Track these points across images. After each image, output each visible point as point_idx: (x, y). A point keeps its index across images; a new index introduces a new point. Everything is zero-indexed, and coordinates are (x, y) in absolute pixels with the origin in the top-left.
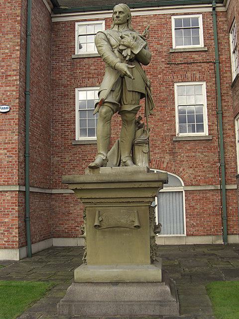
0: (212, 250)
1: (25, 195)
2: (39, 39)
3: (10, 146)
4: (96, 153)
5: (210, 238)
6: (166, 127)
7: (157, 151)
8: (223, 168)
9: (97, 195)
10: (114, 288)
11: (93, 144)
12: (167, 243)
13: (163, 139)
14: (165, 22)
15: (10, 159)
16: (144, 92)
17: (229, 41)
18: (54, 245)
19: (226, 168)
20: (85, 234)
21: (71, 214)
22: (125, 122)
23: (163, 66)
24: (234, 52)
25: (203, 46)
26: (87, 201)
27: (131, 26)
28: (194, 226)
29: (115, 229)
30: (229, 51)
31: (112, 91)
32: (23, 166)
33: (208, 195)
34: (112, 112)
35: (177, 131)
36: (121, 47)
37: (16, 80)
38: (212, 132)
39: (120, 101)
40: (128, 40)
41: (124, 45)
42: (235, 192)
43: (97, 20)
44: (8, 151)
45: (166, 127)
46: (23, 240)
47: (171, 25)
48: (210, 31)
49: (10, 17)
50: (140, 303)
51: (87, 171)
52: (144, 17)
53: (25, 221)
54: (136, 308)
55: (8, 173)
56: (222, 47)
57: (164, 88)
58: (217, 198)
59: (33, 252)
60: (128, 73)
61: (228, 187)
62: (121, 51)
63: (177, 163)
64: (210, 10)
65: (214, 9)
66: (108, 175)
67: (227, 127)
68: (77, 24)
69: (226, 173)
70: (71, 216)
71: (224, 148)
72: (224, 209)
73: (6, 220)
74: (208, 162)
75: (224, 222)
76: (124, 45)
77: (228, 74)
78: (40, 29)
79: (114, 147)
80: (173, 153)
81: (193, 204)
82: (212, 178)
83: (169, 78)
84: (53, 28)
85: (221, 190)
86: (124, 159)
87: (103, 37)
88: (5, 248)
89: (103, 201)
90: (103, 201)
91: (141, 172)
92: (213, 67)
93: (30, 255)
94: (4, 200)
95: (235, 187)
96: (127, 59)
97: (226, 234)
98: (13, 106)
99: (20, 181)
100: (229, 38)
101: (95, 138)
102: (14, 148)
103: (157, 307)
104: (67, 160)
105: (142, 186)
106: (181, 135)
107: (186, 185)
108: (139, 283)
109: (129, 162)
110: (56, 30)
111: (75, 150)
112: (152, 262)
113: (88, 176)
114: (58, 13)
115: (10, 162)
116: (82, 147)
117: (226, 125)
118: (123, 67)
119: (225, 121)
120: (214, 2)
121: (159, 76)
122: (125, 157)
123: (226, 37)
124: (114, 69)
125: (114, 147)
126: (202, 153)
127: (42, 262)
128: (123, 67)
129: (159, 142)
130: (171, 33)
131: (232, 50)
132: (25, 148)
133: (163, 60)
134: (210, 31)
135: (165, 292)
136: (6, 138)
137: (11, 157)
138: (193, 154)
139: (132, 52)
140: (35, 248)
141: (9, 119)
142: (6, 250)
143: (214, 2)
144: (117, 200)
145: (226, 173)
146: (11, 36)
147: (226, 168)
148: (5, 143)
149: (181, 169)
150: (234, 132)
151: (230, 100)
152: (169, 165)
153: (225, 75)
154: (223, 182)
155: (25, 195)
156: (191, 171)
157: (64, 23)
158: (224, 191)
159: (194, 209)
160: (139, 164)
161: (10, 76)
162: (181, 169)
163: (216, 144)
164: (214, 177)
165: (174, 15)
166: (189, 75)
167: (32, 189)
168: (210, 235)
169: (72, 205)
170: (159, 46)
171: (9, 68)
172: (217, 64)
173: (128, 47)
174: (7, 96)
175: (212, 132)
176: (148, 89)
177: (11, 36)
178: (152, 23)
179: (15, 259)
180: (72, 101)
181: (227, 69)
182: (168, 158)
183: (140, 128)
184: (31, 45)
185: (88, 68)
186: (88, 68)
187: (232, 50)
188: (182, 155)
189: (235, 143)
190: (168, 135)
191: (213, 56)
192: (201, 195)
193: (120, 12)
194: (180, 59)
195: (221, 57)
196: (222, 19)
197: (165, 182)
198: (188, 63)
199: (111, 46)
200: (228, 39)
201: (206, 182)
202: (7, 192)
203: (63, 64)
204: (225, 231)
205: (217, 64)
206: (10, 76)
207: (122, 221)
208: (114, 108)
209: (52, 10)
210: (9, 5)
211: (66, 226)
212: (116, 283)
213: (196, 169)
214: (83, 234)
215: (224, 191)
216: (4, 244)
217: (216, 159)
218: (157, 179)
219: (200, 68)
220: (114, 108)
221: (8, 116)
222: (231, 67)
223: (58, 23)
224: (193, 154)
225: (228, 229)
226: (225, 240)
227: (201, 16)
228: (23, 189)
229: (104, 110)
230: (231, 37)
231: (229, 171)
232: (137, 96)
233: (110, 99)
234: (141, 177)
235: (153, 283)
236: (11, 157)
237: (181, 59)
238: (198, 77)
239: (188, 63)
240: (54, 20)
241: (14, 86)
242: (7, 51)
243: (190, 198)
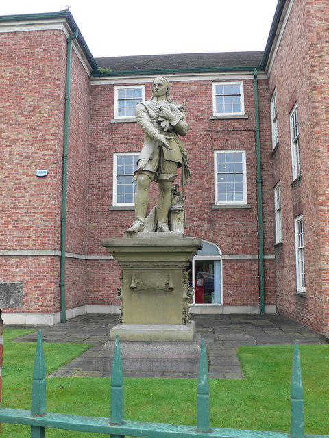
0: (246, 319)
1: (61, 259)
2: (78, 102)
3: (47, 210)
4: (134, 219)
5: (247, 307)
6: (205, 195)
7: (195, 219)
8: (261, 237)
9: (134, 259)
10: (147, 346)
11: (131, 211)
12: (203, 312)
13: (202, 207)
14: (206, 89)
15: (47, 224)
16: (181, 161)
17: (270, 109)
18: (88, 312)
19: (264, 238)
20: (121, 295)
21: (106, 281)
22: (163, 190)
23: (204, 133)
24: (275, 121)
25: (244, 114)
26: (123, 264)
27: (170, 97)
28: (231, 296)
29: (151, 291)
30: (270, 119)
31: (150, 160)
32: (59, 230)
33: (246, 264)
34: (150, 180)
35: (216, 200)
36: (160, 119)
37: (54, 144)
38: (251, 201)
39: (157, 170)
40: (167, 111)
41: (163, 117)
42: (273, 262)
43: (137, 84)
44: (44, 216)
45: (205, 195)
46: (57, 305)
47: (211, 92)
48: (251, 99)
49: (49, 81)
50: (171, 360)
51: (125, 236)
52: (184, 83)
53: (60, 286)
54: (168, 365)
55: (45, 237)
56: (263, 115)
57: (204, 155)
58: (255, 267)
59: (67, 318)
60: (167, 144)
61: (267, 257)
62: (159, 123)
63: (215, 232)
64: (252, 77)
65: (255, 76)
66: (144, 240)
67: (267, 196)
68: (116, 88)
69: (264, 243)
70: (106, 283)
71: (263, 217)
72: (262, 279)
73: (41, 285)
74: (246, 231)
75: (262, 292)
76: (163, 117)
77: (269, 143)
78: (79, 93)
79: (151, 213)
80: (211, 221)
81: (230, 273)
82: (250, 247)
83: (209, 145)
84: (92, 90)
85: (259, 259)
86: (160, 225)
87: (143, 108)
88: (39, 313)
89: (139, 264)
90: (139, 264)
91: (175, 237)
92: (253, 136)
93: (63, 321)
94: (39, 265)
95: (272, 257)
96: (165, 130)
97: (264, 303)
98: (50, 170)
99: (56, 245)
100: (270, 106)
101: (132, 204)
102: (50, 213)
103: (188, 365)
104: (103, 226)
105: (171, 251)
106: (220, 203)
107: (223, 254)
108: (171, 341)
109: (166, 228)
110: (95, 93)
111: (111, 216)
112: (185, 322)
113: (127, 241)
114: (97, 77)
115: (47, 226)
116: (120, 213)
117: (266, 194)
118: (162, 137)
119: (265, 189)
120: (255, 69)
121: (199, 143)
122: (162, 224)
123: (268, 105)
124: (152, 139)
125: (151, 213)
126: (240, 221)
127: (76, 327)
128: (162, 137)
129: (197, 210)
130: (212, 100)
131: (273, 119)
132: (62, 213)
133: (203, 127)
134: (251, 99)
135: (195, 351)
136: (43, 202)
137: (48, 221)
138: (232, 223)
139: (170, 124)
140: (70, 314)
141: (46, 184)
142: (40, 315)
143: (255, 69)
144: (153, 264)
145: (264, 243)
146: (50, 100)
147: (264, 238)
148: (42, 208)
149: (219, 238)
150: (273, 201)
151: (270, 169)
152: (207, 233)
153: (266, 143)
154: (262, 252)
155: (61, 259)
156: (229, 240)
157: (104, 86)
158: (262, 260)
159: (232, 278)
160: (175, 230)
161: (48, 140)
162: (219, 238)
163: (255, 213)
164: (252, 247)
165: (214, 81)
166: (229, 142)
167: (67, 255)
168: (247, 305)
169: (107, 272)
170: (200, 113)
171: (47, 132)
172: (258, 132)
173: (166, 119)
174: (45, 160)
175: (251, 201)
176: (184, 159)
177: (50, 100)
178: (193, 89)
179: (49, 324)
180: (109, 166)
181: (268, 138)
182: (206, 226)
183: (176, 195)
184: (70, 109)
185: (127, 133)
186: (127, 133)
187: (273, 119)
188: (221, 222)
189: (274, 212)
190: (207, 203)
191: (254, 124)
192: (239, 264)
193: (159, 85)
194: (220, 127)
195: (262, 125)
196: (263, 87)
197: (199, 248)
198: (228, 131)
199: (151, 117)
200: (269, 107)
201: (245, 252)
202: (42, 256)
203: (101, 128)
204: (262, 301)
205: (258, 132)
206: (48, 140)
207: (158, 283)
208: (152, 176)
209: (91, 73)
210: (48, 68)
211: (101, 293)
212: (149, 342)
213: (234, 238)
214: (119, 295)
215: (262, 260)
216: (38, 309)
217: (255, 228)
218: (191, 244)
219: (240, 136)
220: (152, 176)
221: (45, 181)
222: (271, 135)
223: (96, 87)
224: (232, 223)
225: (265, 299)
226: (262, 310)
227: (242, 83)
228: (59, 253)
229: (142, 178)
230: (272, 105)
231: (268, 240)
232: (175, 166)
233: (149, 168)
234: (176, 242)
235: (185, 342)
236: (48, 221)
237: (222, 126)
238: (238, 144)
239: (228, 131)
240: (93, 83)
241: (51, 150)
242: (46, 115)
243: (227, 267)
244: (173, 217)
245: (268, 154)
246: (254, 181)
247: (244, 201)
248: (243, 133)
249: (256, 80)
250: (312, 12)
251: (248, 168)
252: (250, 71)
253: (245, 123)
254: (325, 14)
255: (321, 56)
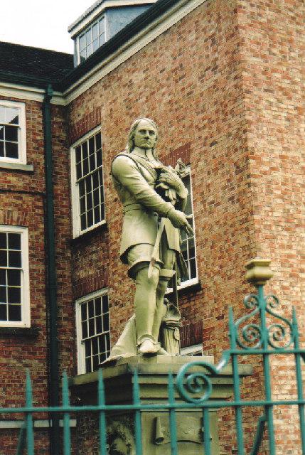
48: (39, 138)
126: (19, 359)
143: (50, 86)
151: (67, 266)
175: (38, 322)
227: (22, 106)
244: (167, 333)
245: (64, 239)
246: (42, 286)
247: (25, 322)
248: (24, 196)
249: (45, 107)
250: (247, 41)
251: (31, 262)
252: (40, 87)
253: (28, 179)
254: (261, 49)
255: (259, 110)
